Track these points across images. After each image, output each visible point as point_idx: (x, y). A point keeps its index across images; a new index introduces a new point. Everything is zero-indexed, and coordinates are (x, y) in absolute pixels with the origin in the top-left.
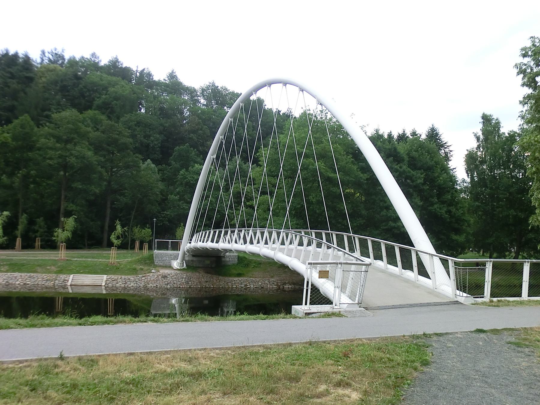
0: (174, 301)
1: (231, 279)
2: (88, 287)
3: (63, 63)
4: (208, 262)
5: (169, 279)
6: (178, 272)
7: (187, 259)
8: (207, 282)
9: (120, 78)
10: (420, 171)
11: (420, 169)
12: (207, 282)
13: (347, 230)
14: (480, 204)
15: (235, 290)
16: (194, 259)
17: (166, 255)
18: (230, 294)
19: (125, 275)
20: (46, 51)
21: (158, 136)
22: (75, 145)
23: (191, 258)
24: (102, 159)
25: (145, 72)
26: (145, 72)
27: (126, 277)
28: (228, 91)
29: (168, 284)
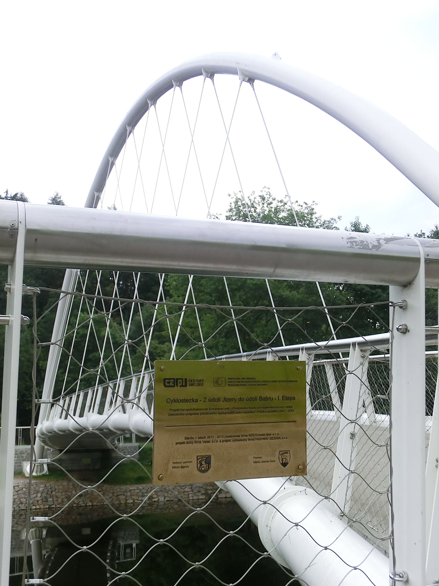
1: (124, 487)
4: (87, 461)
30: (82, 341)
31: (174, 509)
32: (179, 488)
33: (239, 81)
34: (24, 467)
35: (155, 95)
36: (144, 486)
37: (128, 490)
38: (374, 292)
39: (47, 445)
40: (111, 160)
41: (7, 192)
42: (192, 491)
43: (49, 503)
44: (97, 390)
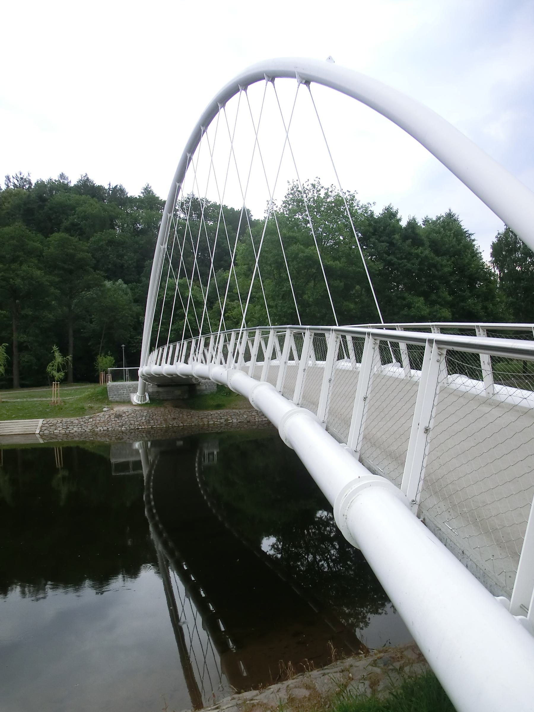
0: (137, 445)
1: (206, 412)
2: (18, 437)
3: (30, 187)
5: (125, 418)
6: (137, 408)
7: (150, 390)
8: (174, 419)
9: (89, 196)
10: (445, 257)
11: (444, 254)
12: (174, 419)
14: (514, 300)
15: (212, 428)
16: (160, 389)
17: (123, 387)
18: (207, 432)
19: (69, 417)
20: (11, 177)
21: (132, 255)
22: (21, 264)
23: (156, 389)
24: (57, 280)
27: (69, 420)
28: (209, 202)
29: (123, 425)
30: (171, 300)
31: (244, 428)
32: (248, 413)
33: (297, 84)
34: (132, 398)
35: (223, 99)
36: (222, 411)
37: (209, 414)
38: (400, 262)
39: (147, 381)
40: (189, 155)
41: (110, 184)
42: (258, 415)
43: (151, 424)
44: (183, 343)
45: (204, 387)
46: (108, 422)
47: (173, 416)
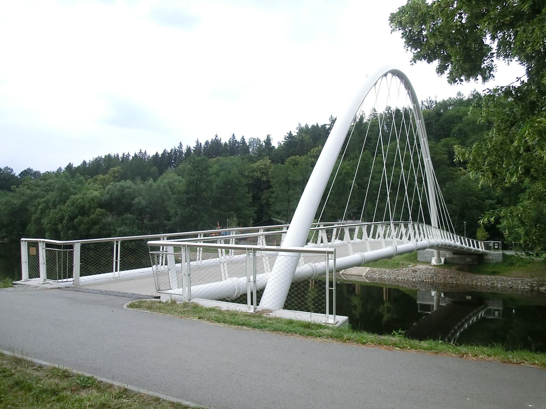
4: (469, 260)
12: (452, 277)
13: (463, 235)
16: (455, 256)
25: (365, 121)
26: (365, 121)
45: (491, 257)
46: (407, 274)
47: (451, 276)
